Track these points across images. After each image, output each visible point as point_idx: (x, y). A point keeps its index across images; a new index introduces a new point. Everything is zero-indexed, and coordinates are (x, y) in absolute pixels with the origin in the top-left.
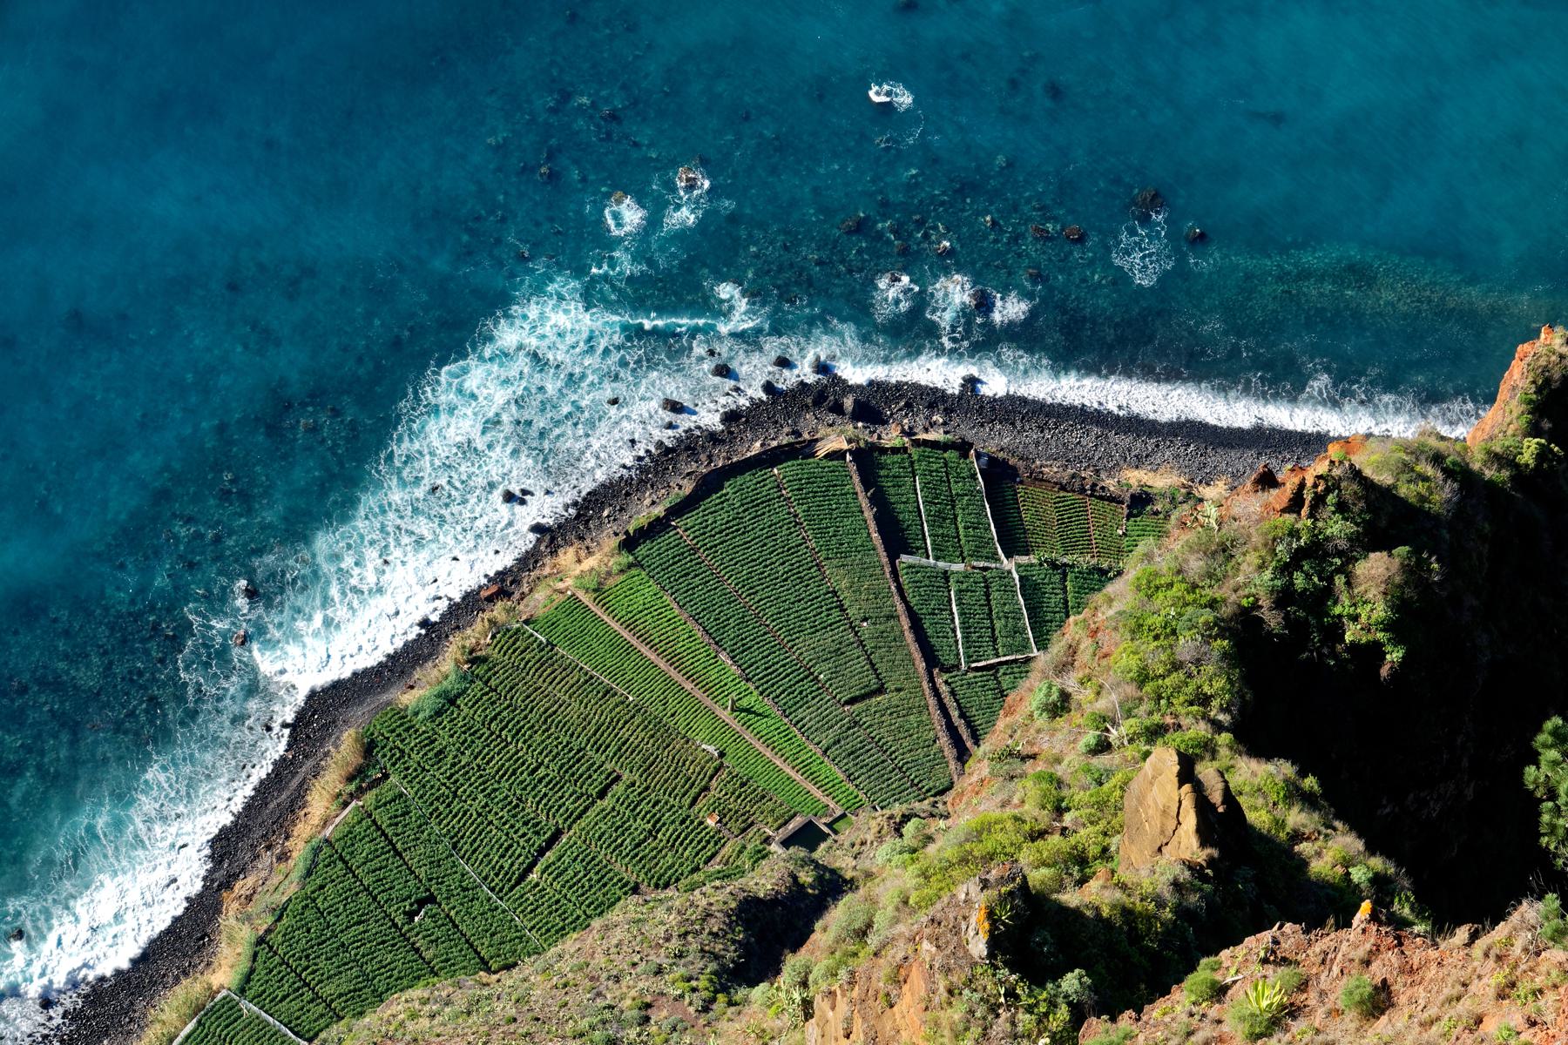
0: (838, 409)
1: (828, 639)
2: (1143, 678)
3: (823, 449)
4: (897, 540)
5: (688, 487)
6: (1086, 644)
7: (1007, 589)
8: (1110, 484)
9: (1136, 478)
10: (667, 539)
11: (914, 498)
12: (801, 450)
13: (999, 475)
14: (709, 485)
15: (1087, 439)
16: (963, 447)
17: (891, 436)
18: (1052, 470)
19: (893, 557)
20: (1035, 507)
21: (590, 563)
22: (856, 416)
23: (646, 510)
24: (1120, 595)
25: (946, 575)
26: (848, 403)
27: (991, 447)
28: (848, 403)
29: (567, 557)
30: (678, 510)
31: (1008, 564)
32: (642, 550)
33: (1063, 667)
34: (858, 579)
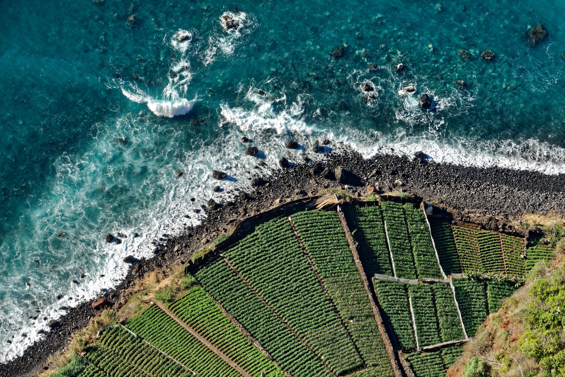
0: (331, 176)
1: (327, 332)
2: (539, 355)
3: (321, 203)
4: (372, 265)
5: (231, 230)
6: (501, 332)
7: (447, 296)
8: (515, 224)
9: (532, 220)
10: (217, 266)
11: (382, 235)
12: (306, 204)
13: (440, 219)
14: (245, 229)
15: (498, 193)
16: (416, 201)
17: (368, 194)
18: (476, 216)
19: (369, 276)
20: (466, 240)
21: (166, 282)
22: (343, 181)
23: (200, 250)
24: (524, 299)
25: (405, 288)
26: (338, 171)
27: (435, 201)
28: (338, 171)
29: (150, 278)
30: (224, 246)
31: (446, 279)
32: (200, 273)
33: (485, 349)
34: (346, 289)
